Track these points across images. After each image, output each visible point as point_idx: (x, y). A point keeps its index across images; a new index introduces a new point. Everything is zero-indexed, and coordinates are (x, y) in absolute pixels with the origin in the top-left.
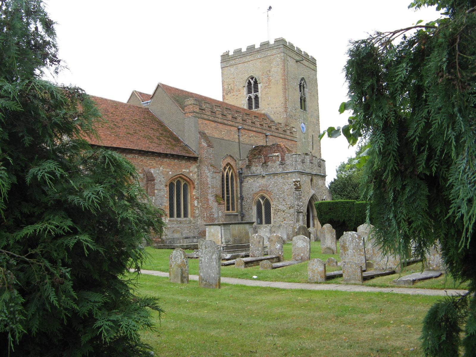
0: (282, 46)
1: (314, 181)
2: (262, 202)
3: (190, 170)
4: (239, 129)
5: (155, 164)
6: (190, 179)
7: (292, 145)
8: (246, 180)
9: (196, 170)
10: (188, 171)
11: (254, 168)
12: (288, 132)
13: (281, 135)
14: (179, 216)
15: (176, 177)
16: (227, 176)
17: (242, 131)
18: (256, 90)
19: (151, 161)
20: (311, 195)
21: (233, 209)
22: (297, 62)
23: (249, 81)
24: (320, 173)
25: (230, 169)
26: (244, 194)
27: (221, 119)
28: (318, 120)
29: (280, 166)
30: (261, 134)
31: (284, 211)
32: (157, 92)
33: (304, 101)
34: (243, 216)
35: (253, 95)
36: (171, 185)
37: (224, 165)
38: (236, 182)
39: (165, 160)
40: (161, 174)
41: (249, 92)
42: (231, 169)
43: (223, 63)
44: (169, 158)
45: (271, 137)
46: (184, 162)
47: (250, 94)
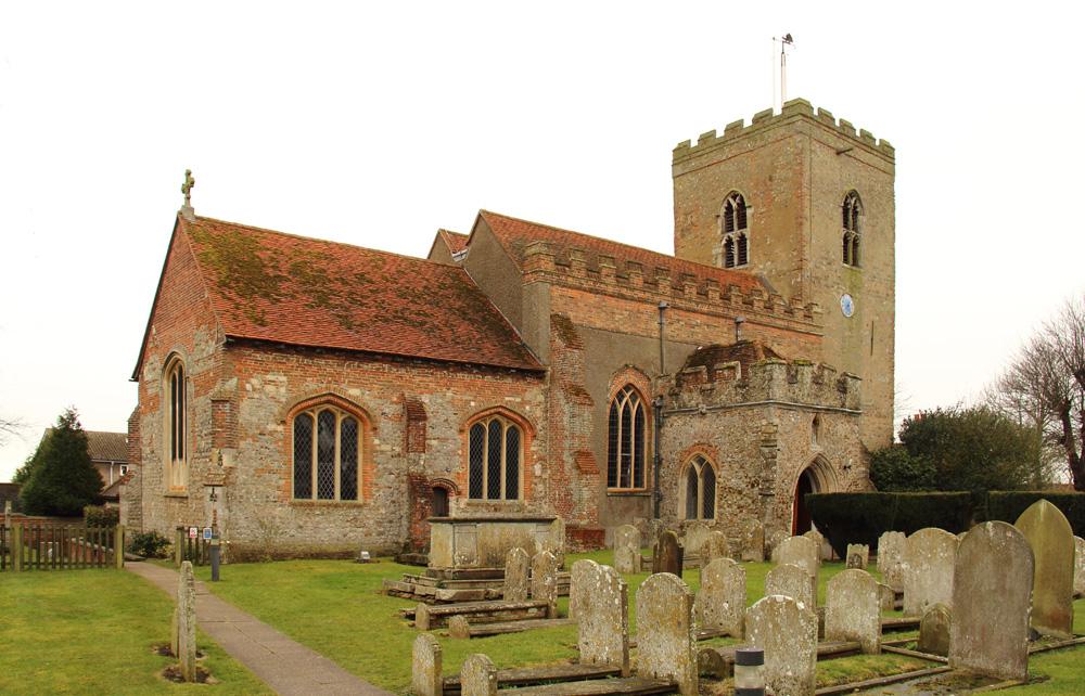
0: (800, 117)
1: (824, 425)
2: (698, 470)
3: (528, 400)
4: (661, 309)
5: (432, 385)
6: (523, 418)
7: (808, 345)
8: (668, 422)
9: (541, 398)
10: (518, 400)
11: (685, 396)
12: (799, 315)
13: (779, 323)
14: (494, 494)
15: (488, 413)
16: (627, 411)
17: (670, 313)
18: (742, 225)
19: (424, 379)
20: (812, 456)
21: (638, 483)
22: (838, 153)
23: (729, 203)
24: (843, 405)
25: (633, 398)
26: (664, 453)
27: (614, 286)
28: (892, 289)
29: (738, 389)
30: (722, 321)
31: (740, 492)
32: (478, 229)
33: (855, 245)
34: (659, 500)
35: (734, 235)
36: (477, 431)
37: (620, 387)
38: (650, 426)
39: (460, 375)
40: (449, 406)
41: (729, 228)
42: (637, 398)
43: (676, 167)
44: (470, 372)
45: (750, 326)
46: (509, 380)
47: (730, 234)
